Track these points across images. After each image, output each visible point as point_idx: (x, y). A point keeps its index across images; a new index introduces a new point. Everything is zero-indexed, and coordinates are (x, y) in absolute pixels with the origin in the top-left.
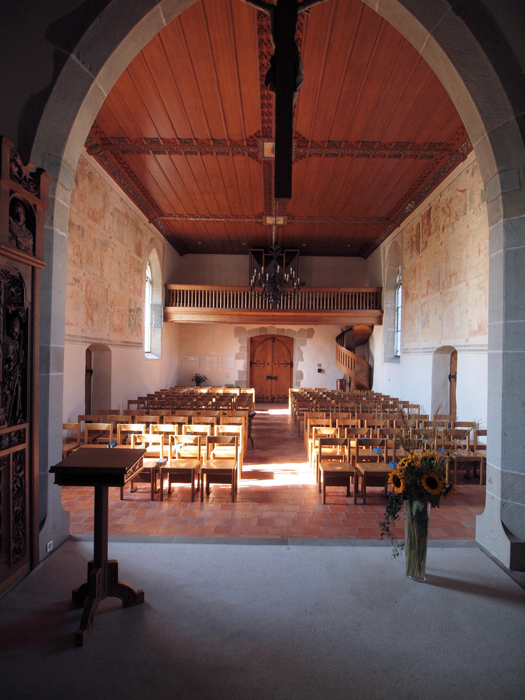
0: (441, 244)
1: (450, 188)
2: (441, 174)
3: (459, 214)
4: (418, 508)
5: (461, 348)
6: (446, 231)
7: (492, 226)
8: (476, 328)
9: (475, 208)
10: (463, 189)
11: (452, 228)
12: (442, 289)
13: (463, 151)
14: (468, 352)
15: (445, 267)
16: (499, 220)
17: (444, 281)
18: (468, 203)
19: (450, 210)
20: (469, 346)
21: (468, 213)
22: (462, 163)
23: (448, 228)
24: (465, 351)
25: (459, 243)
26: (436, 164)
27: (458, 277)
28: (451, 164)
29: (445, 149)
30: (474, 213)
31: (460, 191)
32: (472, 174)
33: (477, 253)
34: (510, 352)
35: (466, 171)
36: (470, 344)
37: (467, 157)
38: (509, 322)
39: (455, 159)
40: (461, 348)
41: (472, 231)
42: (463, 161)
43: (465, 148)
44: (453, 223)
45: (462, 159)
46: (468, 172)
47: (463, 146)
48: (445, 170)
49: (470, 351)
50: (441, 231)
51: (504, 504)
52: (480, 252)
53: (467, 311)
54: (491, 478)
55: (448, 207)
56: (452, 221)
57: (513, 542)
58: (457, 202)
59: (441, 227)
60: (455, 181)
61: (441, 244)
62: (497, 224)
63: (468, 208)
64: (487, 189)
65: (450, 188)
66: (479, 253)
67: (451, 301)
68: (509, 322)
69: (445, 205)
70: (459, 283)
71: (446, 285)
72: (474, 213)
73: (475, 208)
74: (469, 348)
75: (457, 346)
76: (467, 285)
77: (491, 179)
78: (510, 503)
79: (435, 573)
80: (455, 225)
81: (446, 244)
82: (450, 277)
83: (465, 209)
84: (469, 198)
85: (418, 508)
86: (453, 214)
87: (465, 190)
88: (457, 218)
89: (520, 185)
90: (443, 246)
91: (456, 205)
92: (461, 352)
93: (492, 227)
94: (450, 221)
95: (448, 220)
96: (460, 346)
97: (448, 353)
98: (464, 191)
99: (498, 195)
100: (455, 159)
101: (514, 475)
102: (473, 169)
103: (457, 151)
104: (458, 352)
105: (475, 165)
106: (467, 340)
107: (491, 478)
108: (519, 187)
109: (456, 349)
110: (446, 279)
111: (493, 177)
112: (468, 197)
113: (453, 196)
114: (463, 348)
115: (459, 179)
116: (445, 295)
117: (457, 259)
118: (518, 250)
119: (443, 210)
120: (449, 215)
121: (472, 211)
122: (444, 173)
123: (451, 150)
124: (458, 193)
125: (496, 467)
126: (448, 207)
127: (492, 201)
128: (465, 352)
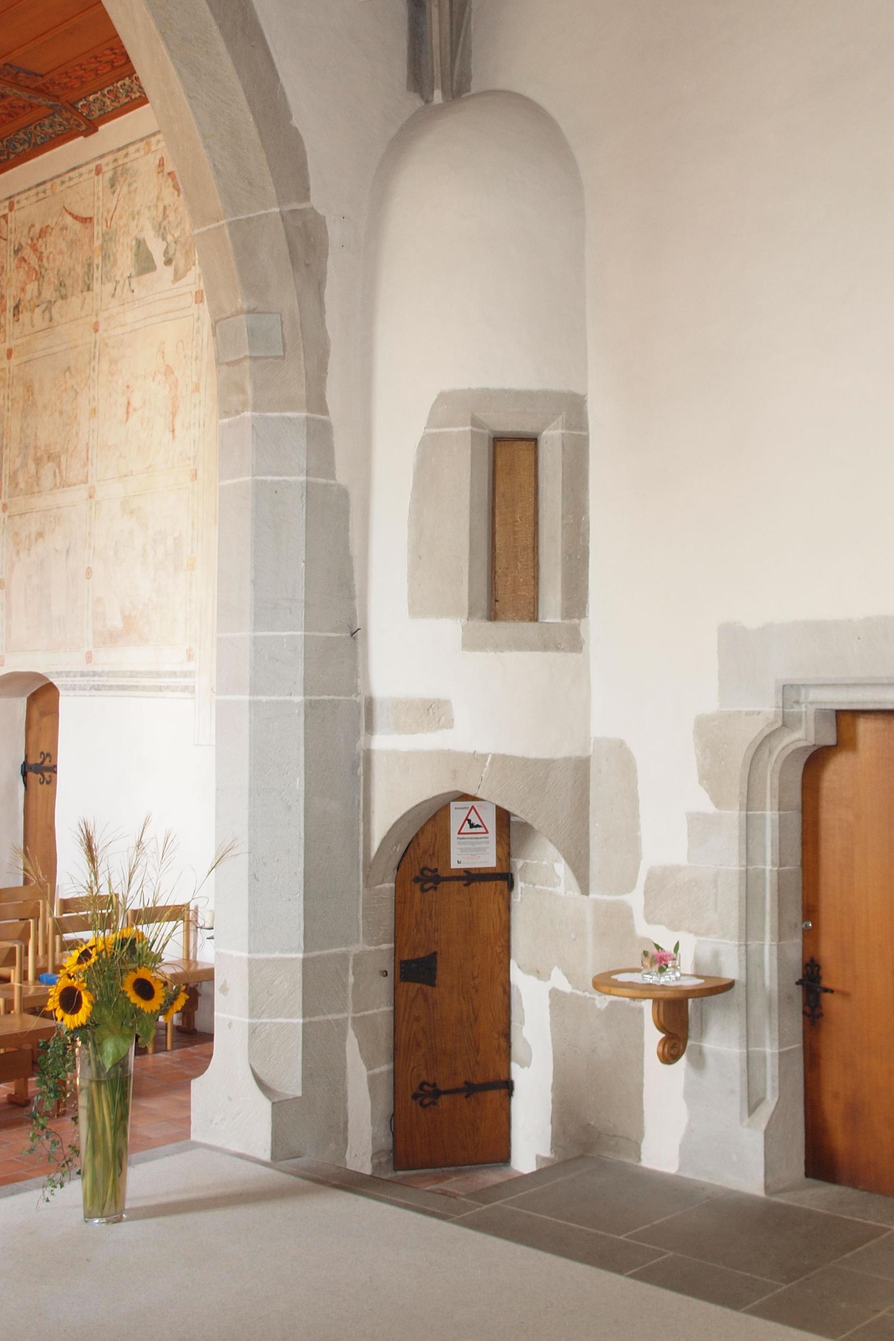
0: (10, 353)
1: (41, 195)
2: (18, 145)
3: (68, 282)
4: (119, 1053)
5: (69, 681)
6: (25, 317)
7: (225, 417)
8: (117, 622)
9: (117, 282)
10: (85, 215)
11: (47, 316)
12: (10, 496)
13: (90, 111)
14: (93, 692)
15: (22, 429)
16: (243, 411)
17: (15, 472)
18: (98, 260)
19: (40, 259)
20: (95, 674)
21: (96, 286)
22: (82, 138)
23: (32, 311)
24: (83, 688)
25: (69, 368)
26: (10, 115)
27: (63, 466)
28: (50, 131)
29: (42, 91)
30: (113, 296)
31: (76, 218)
32: (113, 183)
33: (121, 412)
34: (264, 698)
35: (93, 166)
36: (98, 669)
37: (96, 130)
38: (261, 634)
39: (65, 123)
40: (69, 681)
41: (107, 345)
42: (86, 136)
43: (97, 105)
44: (50, 302)
45: (84, 127)
46: (98, 171)
47: (91, 98)
48: (30, 139)
49: (98, 688)
50: (9, 314)
51: (256, 1028)
52: (131, 410)
53: (89, 572)
54: (225, 981)
55: (34, 248)
56: (48, 293)
57: (276, 1101)
58: (63, 245)
59: (10, 304)
60: (58, 181)
61: (10, 353)
62: (238, 417)
63: (97, 274)
64: (218, 335)
65: (41, 195)
66: (128, 413)
67: (40, 535)
68: (261, 634)
69: (25, 241)
70: (65, 484)
71: (22, 485)
72: (113, 296)
73: (117, 282)
74: (97, 681)
75: (59, 674)
76: (91, 497)
77: (228, 318)
78: (266, 1023)
79: (140, 1204)
80: (55, 310)
81: (26, 358)
82: (38, 461)
83: (89, 273)
84: (102, 248)
85: (119, 1053)
86: (51, 276)
87: (91, 219)
88: (63, 291)
89: (284, 351)
90: (14, 361)
91: (61, 252)
92: (71, 693)
93: (226, 420)
94: (40, 294)
95: (32, 288)
96: (68, 674)
97: (21, 695)
98: (86, 221)
99: (242, 356)
100: (65, 123)
101: (274, 960)
102: (115, 173)
103: (73, 105)
104: (61, 693)
105: (120, 162)
106: (89, 657)
107: (225, 981)
108: (282, 354)
109: (56, 682)
110: (24, 465)
111: (233, 315)
112: (97, 243)
113: (51, 222)
114: (79, 681)
115: (71, 179)
116: (21, 515)
117: (61, 413)
118: (278, 482)
119: (16, 252)
120: (39, 276)
121: (110, 287)
122: (26, 146)
123: (58, 97)
124: (69, 220)
125: (236, 953)
126: (34, 248)
127: (228, 364)
128: (82, 693)
